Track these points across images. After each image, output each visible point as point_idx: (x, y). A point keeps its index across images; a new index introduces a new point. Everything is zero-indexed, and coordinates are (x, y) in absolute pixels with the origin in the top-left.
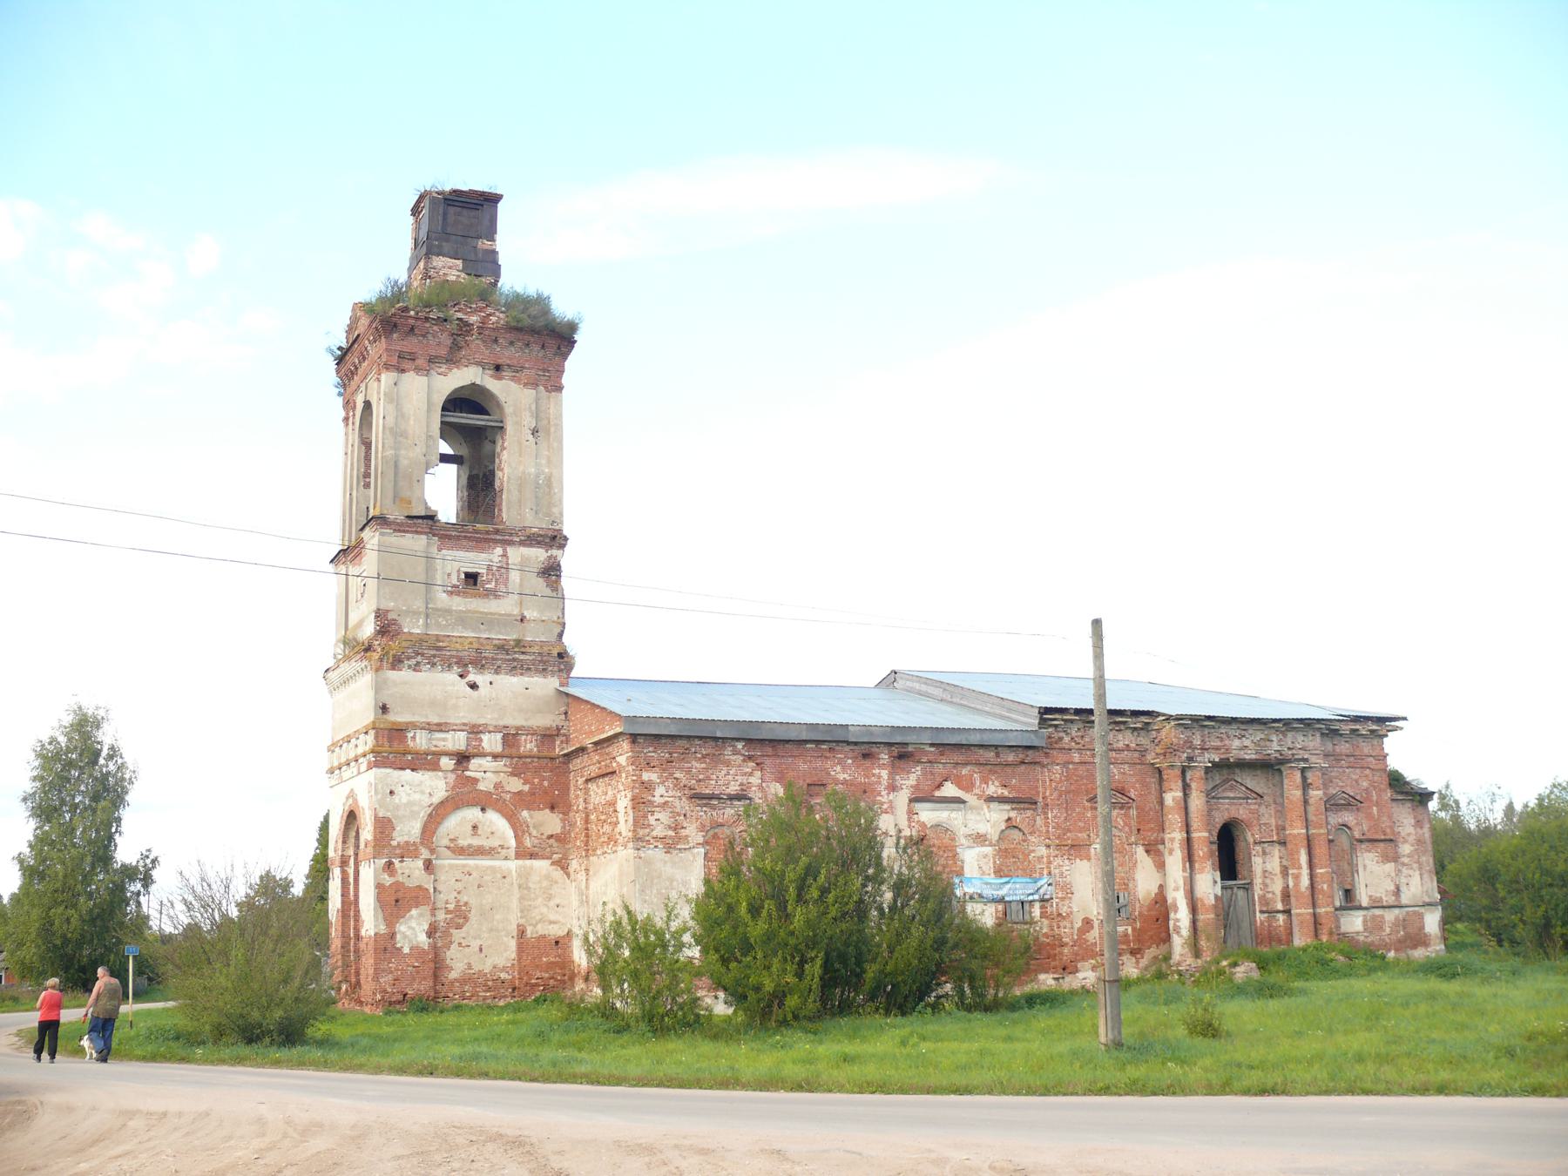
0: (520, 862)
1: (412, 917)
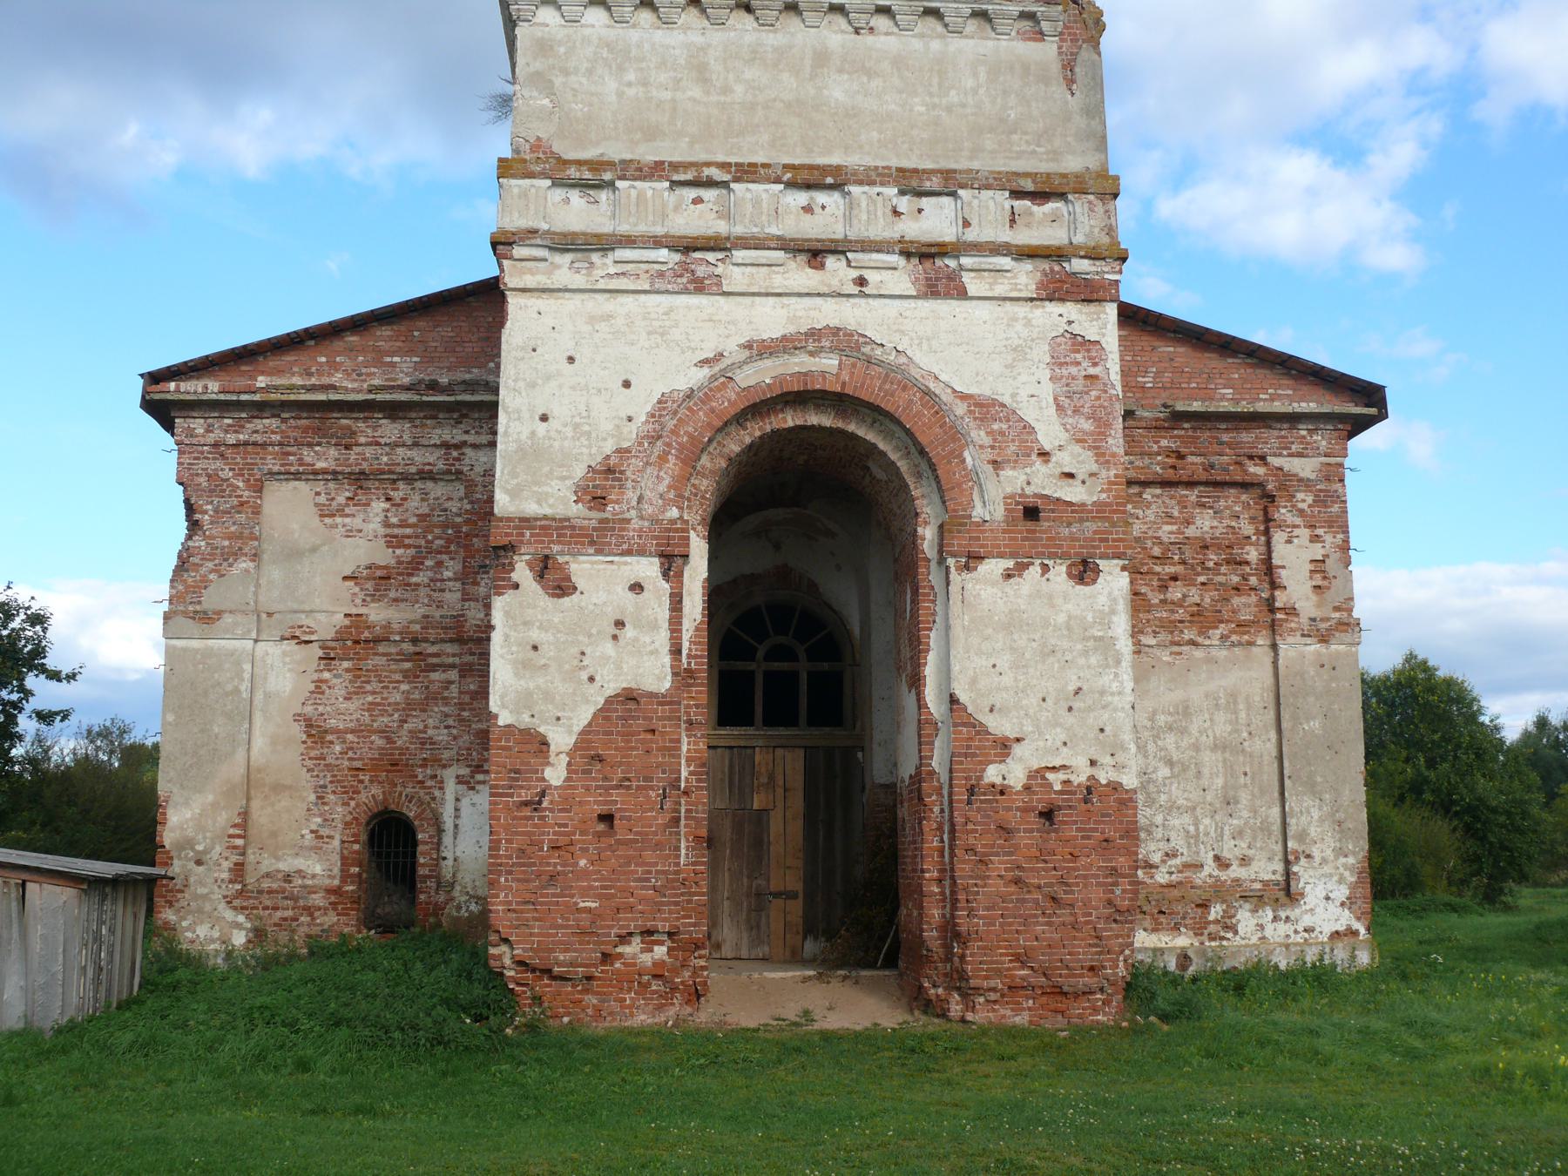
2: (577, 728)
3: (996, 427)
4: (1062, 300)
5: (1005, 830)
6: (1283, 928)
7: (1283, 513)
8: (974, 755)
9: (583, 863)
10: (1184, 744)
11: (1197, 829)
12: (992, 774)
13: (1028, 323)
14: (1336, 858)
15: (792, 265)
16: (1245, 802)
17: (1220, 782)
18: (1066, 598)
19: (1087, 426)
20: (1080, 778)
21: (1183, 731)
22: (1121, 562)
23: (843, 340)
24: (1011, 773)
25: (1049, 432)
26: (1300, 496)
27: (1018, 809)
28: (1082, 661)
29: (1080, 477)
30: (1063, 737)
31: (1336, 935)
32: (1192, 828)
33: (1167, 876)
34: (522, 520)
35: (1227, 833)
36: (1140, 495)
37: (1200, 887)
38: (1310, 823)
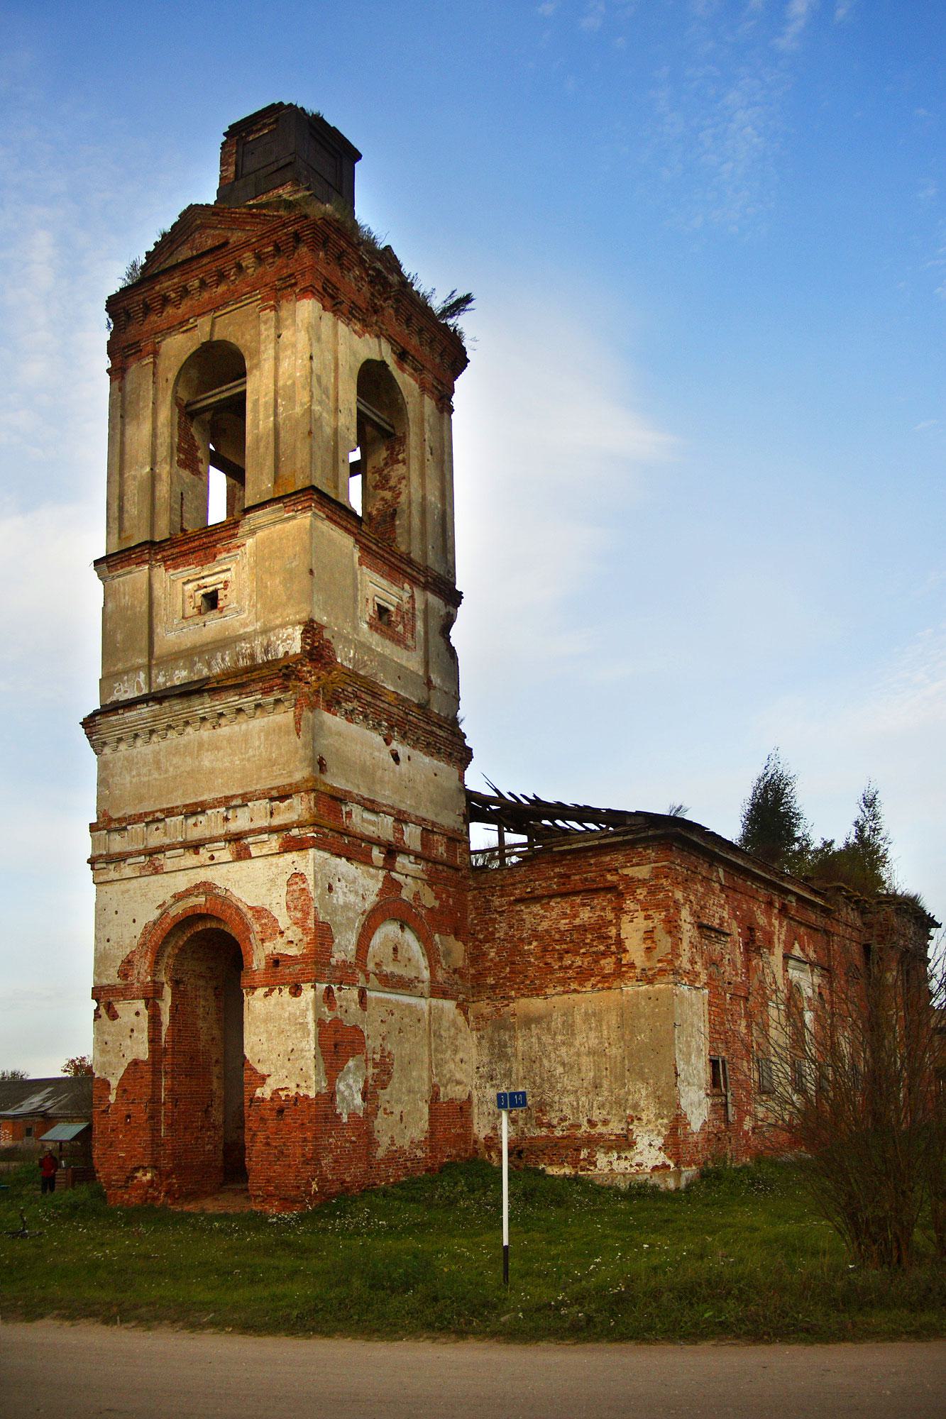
0: (434, 1001)
1: (349, 1071)
2: (119, 1078)
3: (263, 922)
4: (290, 851)
5: (263, 1120)
6: (624, 1164)
7: (629, 905)
8: (253, 1084)
9: (121, 1136)
10: (571, 1053)
11: (578, 1104)
12: (259, 1093)
13: (277, 866)
14: (657, 1120)
15: (187, 854)
16: (606, 1086)
17: (591, 1074)
18: (288, 1004)
19: (299, 915)
20: (292, 1094)
21: (571, 1045)
22: (311, 984)
23: (206, 888)
24: (264, 1092)
25: (284, 921)
26: (639, 891)
27: (269, 1109)
28: (294, 1035)
29: (295, 942)
30: (286, 1074)
31: (655, 1168)
32: (575, 1103)
33: (561, 1133)
34: (102, 987)
35: (595, 1105)
36: (548, 903)
37: (579, 1139)
38: (640, 1098)
